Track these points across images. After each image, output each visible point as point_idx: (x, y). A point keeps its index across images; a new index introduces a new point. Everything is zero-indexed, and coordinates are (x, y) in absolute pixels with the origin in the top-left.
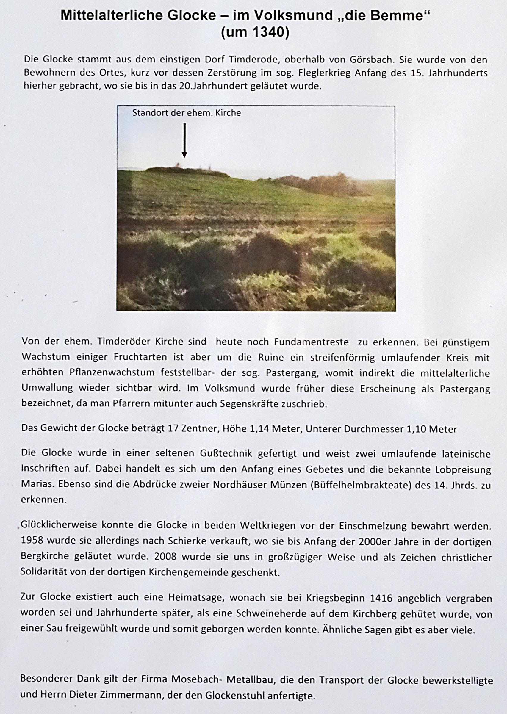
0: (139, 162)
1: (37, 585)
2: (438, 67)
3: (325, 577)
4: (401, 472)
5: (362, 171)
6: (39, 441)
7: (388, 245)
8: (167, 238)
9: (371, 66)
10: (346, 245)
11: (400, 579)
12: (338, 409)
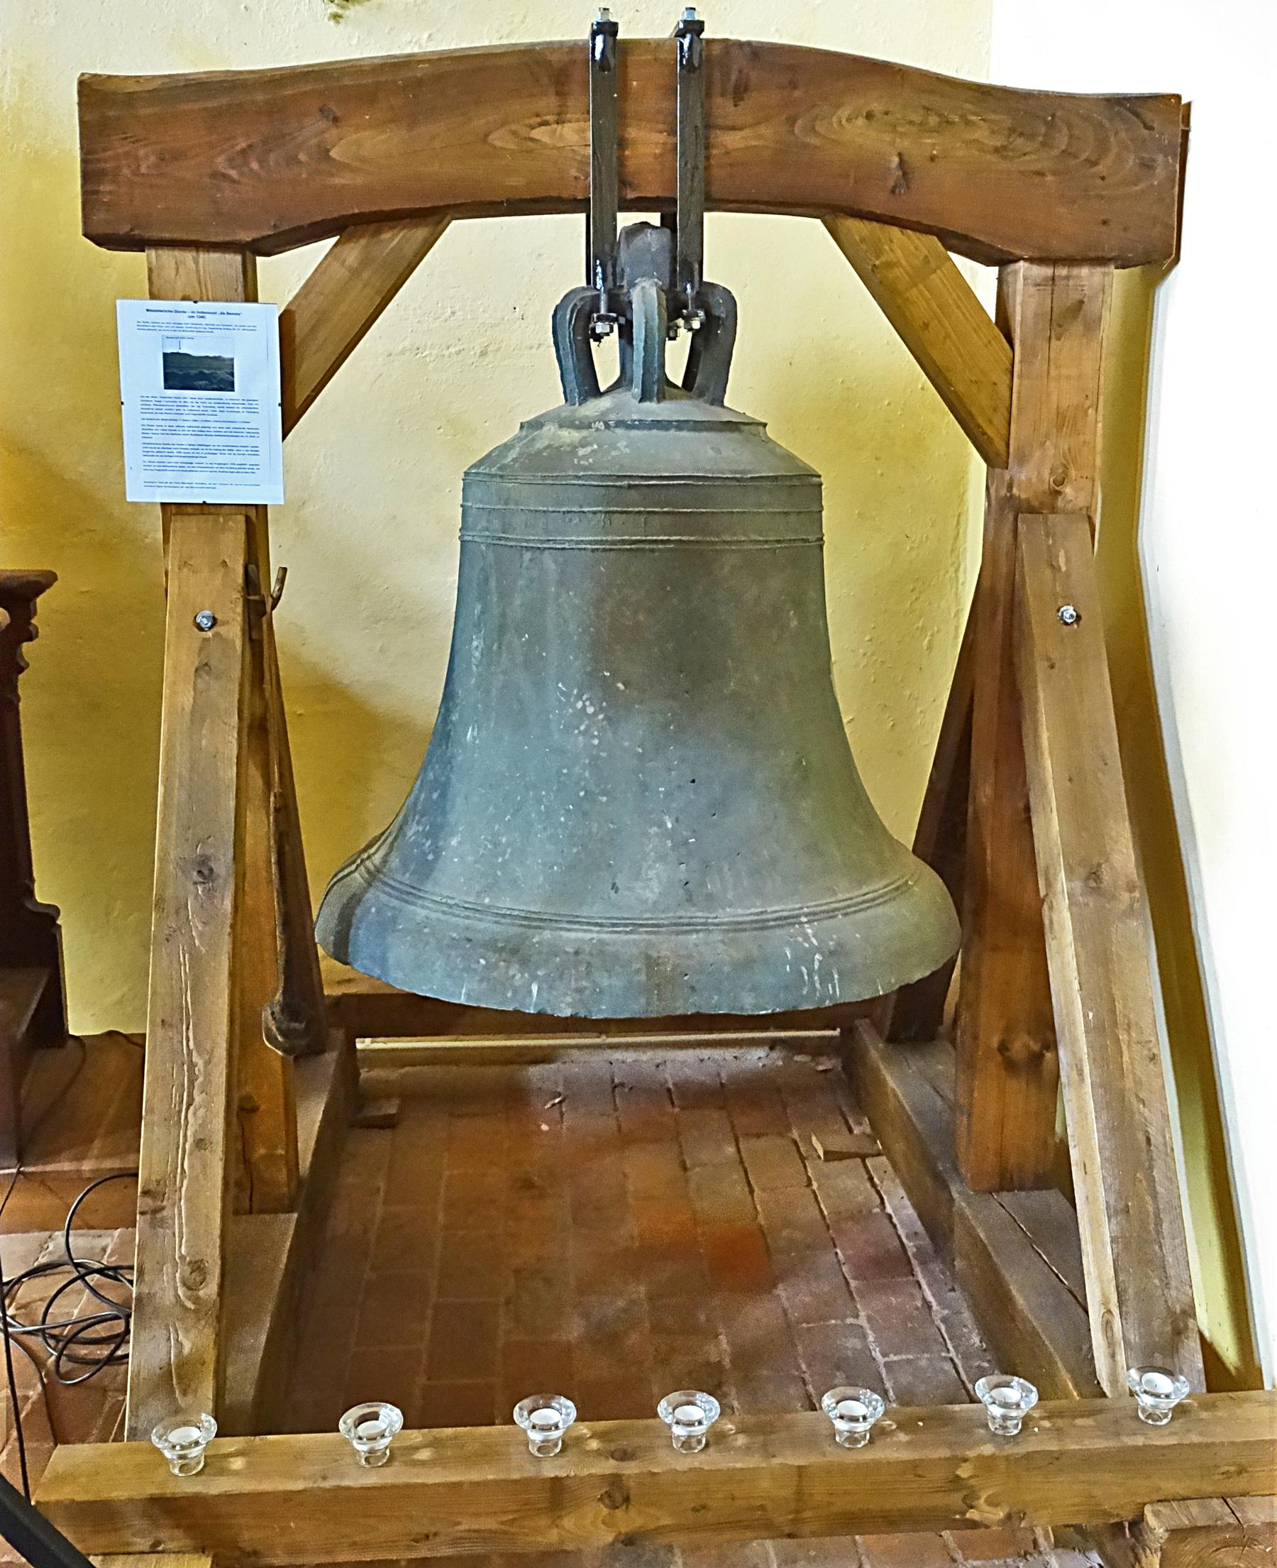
0: (169, 351)
1: (146, 459)
2: (244, 328)
3: (220, 459)
4: (236, 433)
5: (226, 355)
6: (146, 422)
7: (232, 374)
8: (176, 371)
9: (227, 327)
10: (222, 374)
11: (239, 459)
12: (222, 416)
